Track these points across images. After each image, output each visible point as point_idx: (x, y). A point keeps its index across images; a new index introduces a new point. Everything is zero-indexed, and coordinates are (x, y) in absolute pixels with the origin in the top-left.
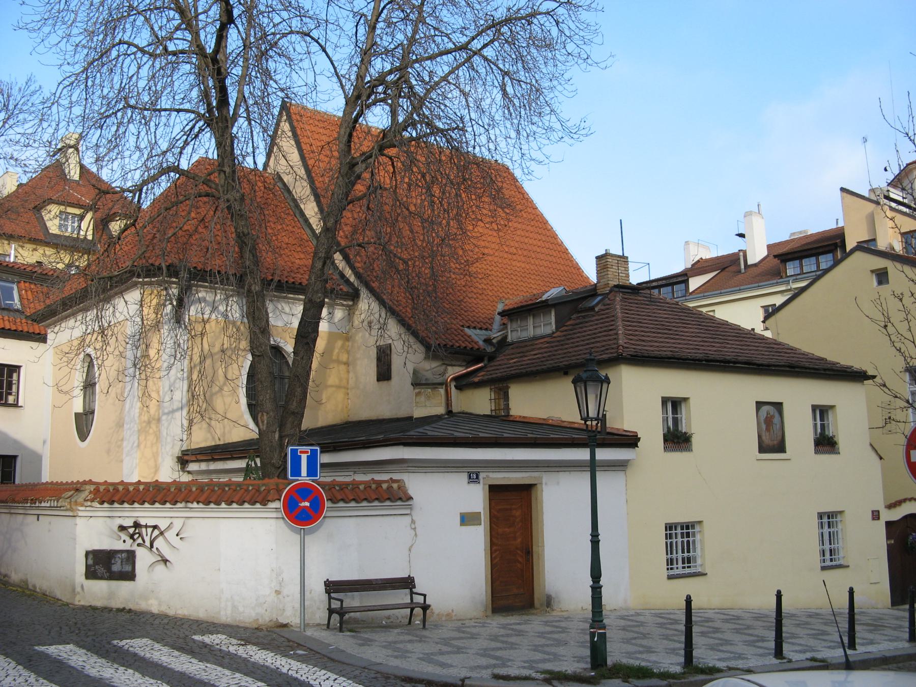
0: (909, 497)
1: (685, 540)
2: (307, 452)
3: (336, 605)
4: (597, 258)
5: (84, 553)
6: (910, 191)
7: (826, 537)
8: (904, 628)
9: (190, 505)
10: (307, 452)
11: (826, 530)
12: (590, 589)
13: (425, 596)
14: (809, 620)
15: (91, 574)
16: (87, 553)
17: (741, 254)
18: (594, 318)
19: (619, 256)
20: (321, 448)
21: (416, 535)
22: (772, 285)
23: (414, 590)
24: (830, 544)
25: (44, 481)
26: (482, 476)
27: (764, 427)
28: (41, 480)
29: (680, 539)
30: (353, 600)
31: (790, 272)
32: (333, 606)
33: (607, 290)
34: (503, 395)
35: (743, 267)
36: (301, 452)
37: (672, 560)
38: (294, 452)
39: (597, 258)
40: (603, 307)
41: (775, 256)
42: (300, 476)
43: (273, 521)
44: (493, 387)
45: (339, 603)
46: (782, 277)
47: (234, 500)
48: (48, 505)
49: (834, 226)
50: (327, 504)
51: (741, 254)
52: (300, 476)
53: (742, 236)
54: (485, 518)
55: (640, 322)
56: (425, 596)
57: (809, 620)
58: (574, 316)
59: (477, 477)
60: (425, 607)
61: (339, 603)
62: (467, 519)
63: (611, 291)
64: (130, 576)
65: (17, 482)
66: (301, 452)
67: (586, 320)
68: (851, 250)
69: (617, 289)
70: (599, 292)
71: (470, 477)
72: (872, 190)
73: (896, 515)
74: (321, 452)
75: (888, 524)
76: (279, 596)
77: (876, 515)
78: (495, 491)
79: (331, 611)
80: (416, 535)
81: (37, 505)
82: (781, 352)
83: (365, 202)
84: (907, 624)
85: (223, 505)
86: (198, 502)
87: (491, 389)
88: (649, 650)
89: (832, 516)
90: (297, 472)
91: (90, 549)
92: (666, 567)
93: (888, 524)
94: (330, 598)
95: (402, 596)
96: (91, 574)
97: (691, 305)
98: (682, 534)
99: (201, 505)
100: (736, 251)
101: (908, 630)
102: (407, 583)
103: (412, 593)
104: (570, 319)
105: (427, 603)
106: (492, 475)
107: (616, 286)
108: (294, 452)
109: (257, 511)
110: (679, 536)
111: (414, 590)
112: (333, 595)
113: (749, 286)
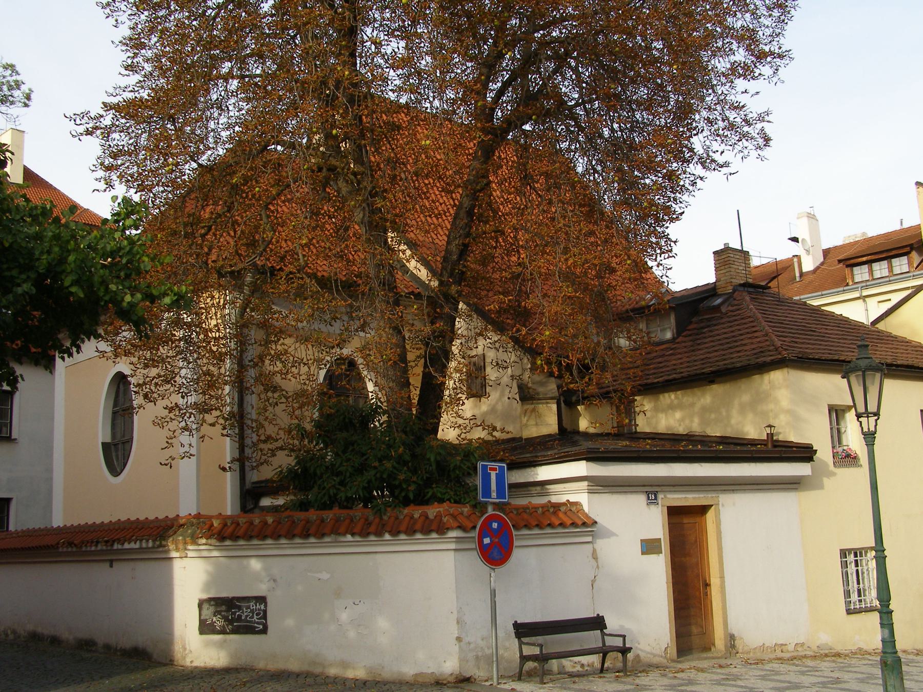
2: (494, 469)
4: (715, 253)
5: (197, 601)
9: (342, 539)
13: (624, 637)
17: (795, 260)
18: (724, 320)
19: (736, 250)
20: (508, 465)
21: (598, 567)
22: (838, 293)
25: (55, 526)
26: (660, 496)
28: (51, 522)
31: (858, 278)
33: (729, 290)
34: (627, 409)
35: (797, 274)
38: (485, 467)
39: (715, 253)
40: (730, 308)
43: (452, 553)
46: (847, 285)
47: (433, 528)
48: (137, 546)
49: (898, 227)
50: (514, 533)
51: (795, 260)
52: (490, 497)
53: (795, 240)
54: (665, 546)
55: (782, 323)
56: (624, 637)
58: (694, 320)
59: (656, 499)
62: (650, 546)
63: (734, 291)
65: (12, 528)
67: (714, 322)
69: (742, 289)
70: (719, 292)
74: (509, 469)
76: (462, 643)
78: (674, 512)
81: (84, 549)
85: (387, 536)
86: (353, 534)
95: (592, 638)
97: (815, 303)
99: (358, 538)
100: (791, 256)
102: (598, 623)
103: (603, 634)
104: (691, 323)
105: (627, 646)
106: (670, 496)
107: (741, 285)
108: (485, 467)
109: (433, 543)
112: (525, 640)
113: (810, 295)
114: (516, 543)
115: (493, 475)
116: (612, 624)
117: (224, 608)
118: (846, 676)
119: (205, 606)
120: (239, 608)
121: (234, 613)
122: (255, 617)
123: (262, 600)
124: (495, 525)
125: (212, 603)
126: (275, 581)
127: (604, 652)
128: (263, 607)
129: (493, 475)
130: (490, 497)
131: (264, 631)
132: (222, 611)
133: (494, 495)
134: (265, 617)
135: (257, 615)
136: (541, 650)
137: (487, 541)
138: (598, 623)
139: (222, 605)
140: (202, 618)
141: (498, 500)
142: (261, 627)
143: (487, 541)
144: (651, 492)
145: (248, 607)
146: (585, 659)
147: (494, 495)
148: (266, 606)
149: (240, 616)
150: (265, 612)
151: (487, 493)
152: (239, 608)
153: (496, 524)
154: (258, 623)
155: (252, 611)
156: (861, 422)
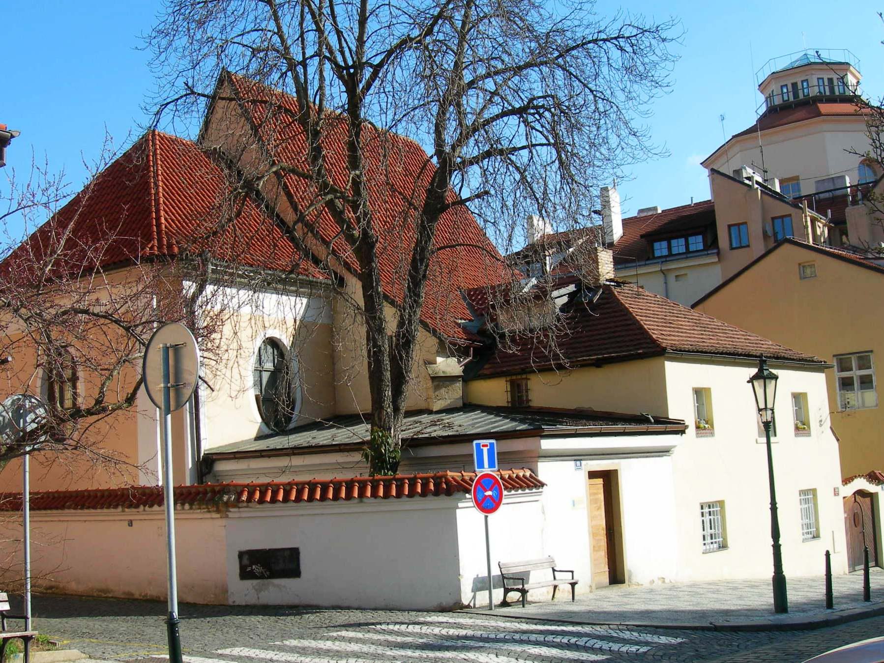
2: (486, 446)
6: (258, 113)
7: (707, 525)
10: (486, 446)
11: (707, 518)
12: (772, 548)
14: (625, 600)
15: (245, 574)
24: (711, 529)
36: (484, 446)
42: (483, 468)
44: (508, 379)
52: (483, 468)
57: (625, 600)
64: (295, 572)
66: (484, 446)
77: (836, 493)
82: (725, 330)
83: (583, 93)
89: (713, 506)
90: (481, 466)
92: (801, 531)
96: (245, 574)
108: (478, 445)
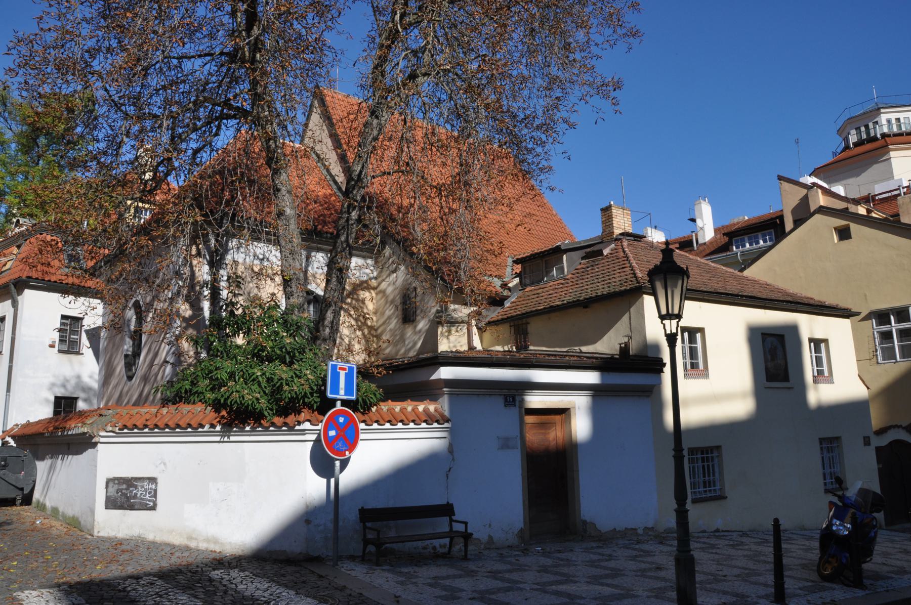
0: (894, 424)
1: (706, 464)
2: (345, 369)
3: (370, 536)
5: (105, 480)
8: (769, 543)
13: (466, 523)
15: (112, 504)
16: (109, 482)
21: (453, 459)
23: (454, 518)
27: (769, 357)
29: (700, 464)
30: (391, 530)
32: (369, 536)
37: (694, 483)
38: (334, 367)
39: (602, 210)
41: (724, 234)
45: (463, 526)
56: (466, 523)
59: (514, 400)
60: (467, 537)
61: (463, 526)
68: (815, 210)
71: (506, 400)
72: (834, 154)
73: (884, 441)
75: (878, 450)
79: (366, 542)
80: (453, 459)
84: (771, 538)
87: (510, 326)
88: (592, 564)
91: (111, 476)
93: (878, 450)
94: (365, 528)
95: (442, 524)
96: (112, 504)
98: (703, 458)
101: (772, 545)
102: (447, 510)
103: (451, 521)
110: (700, 461)
111: (454, 518)
112: (369, 524)
114: (362, 436)
115: (342, 374)
116: (460, 514)
117: (124, 486)
118: (754, 547)
119: (111, 484)
120: (136, 487)
121: (131, 492)
122: (148, 495)
123: (153, 480)
124: (341, 420)
125: (116, 482)
126: (165, 464)
127: (452, 535)
128: (154, 487)
129: (342, 374)
130: (338, 394)
131: (153, 508)
132: (122, 489)
133: (342, 392)
134: (155, 496)
135: (149, 493)
136: (378, 535)
137: (332, 433)
138: (447, 510)
139: (124, 483)
140: (108, 494)
141: (345, 397)
142: (152, 504)
143: (332, 433)
144: (509, 396)
145: (143, 487)
146: (437, 543)
147: (342, 392)
148: (156, 486)
149: (136, 494)
150: (155, 491)
151: (336, 390)
152: (136, 487)
153: (343, 419)
154: (149, 501)
155: (146, 490)
156: (664, 325)
